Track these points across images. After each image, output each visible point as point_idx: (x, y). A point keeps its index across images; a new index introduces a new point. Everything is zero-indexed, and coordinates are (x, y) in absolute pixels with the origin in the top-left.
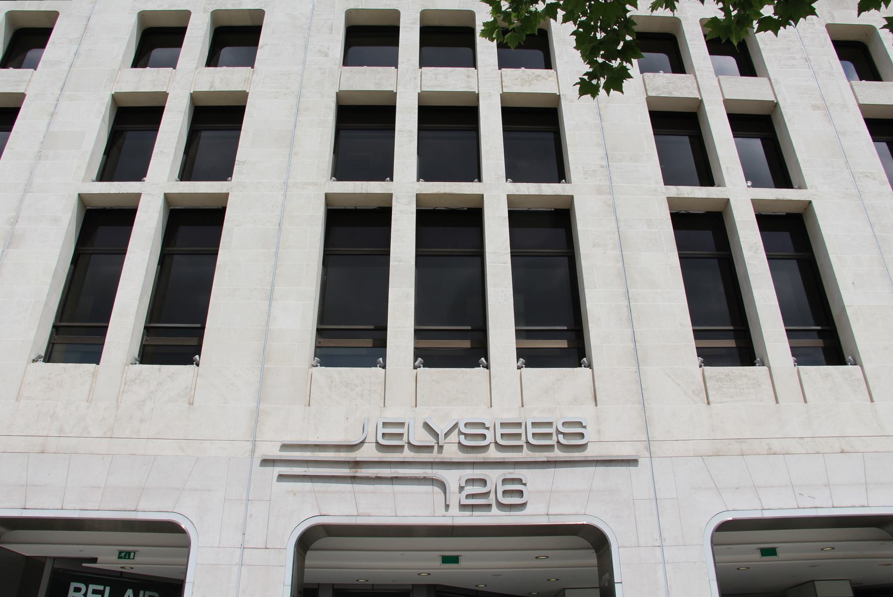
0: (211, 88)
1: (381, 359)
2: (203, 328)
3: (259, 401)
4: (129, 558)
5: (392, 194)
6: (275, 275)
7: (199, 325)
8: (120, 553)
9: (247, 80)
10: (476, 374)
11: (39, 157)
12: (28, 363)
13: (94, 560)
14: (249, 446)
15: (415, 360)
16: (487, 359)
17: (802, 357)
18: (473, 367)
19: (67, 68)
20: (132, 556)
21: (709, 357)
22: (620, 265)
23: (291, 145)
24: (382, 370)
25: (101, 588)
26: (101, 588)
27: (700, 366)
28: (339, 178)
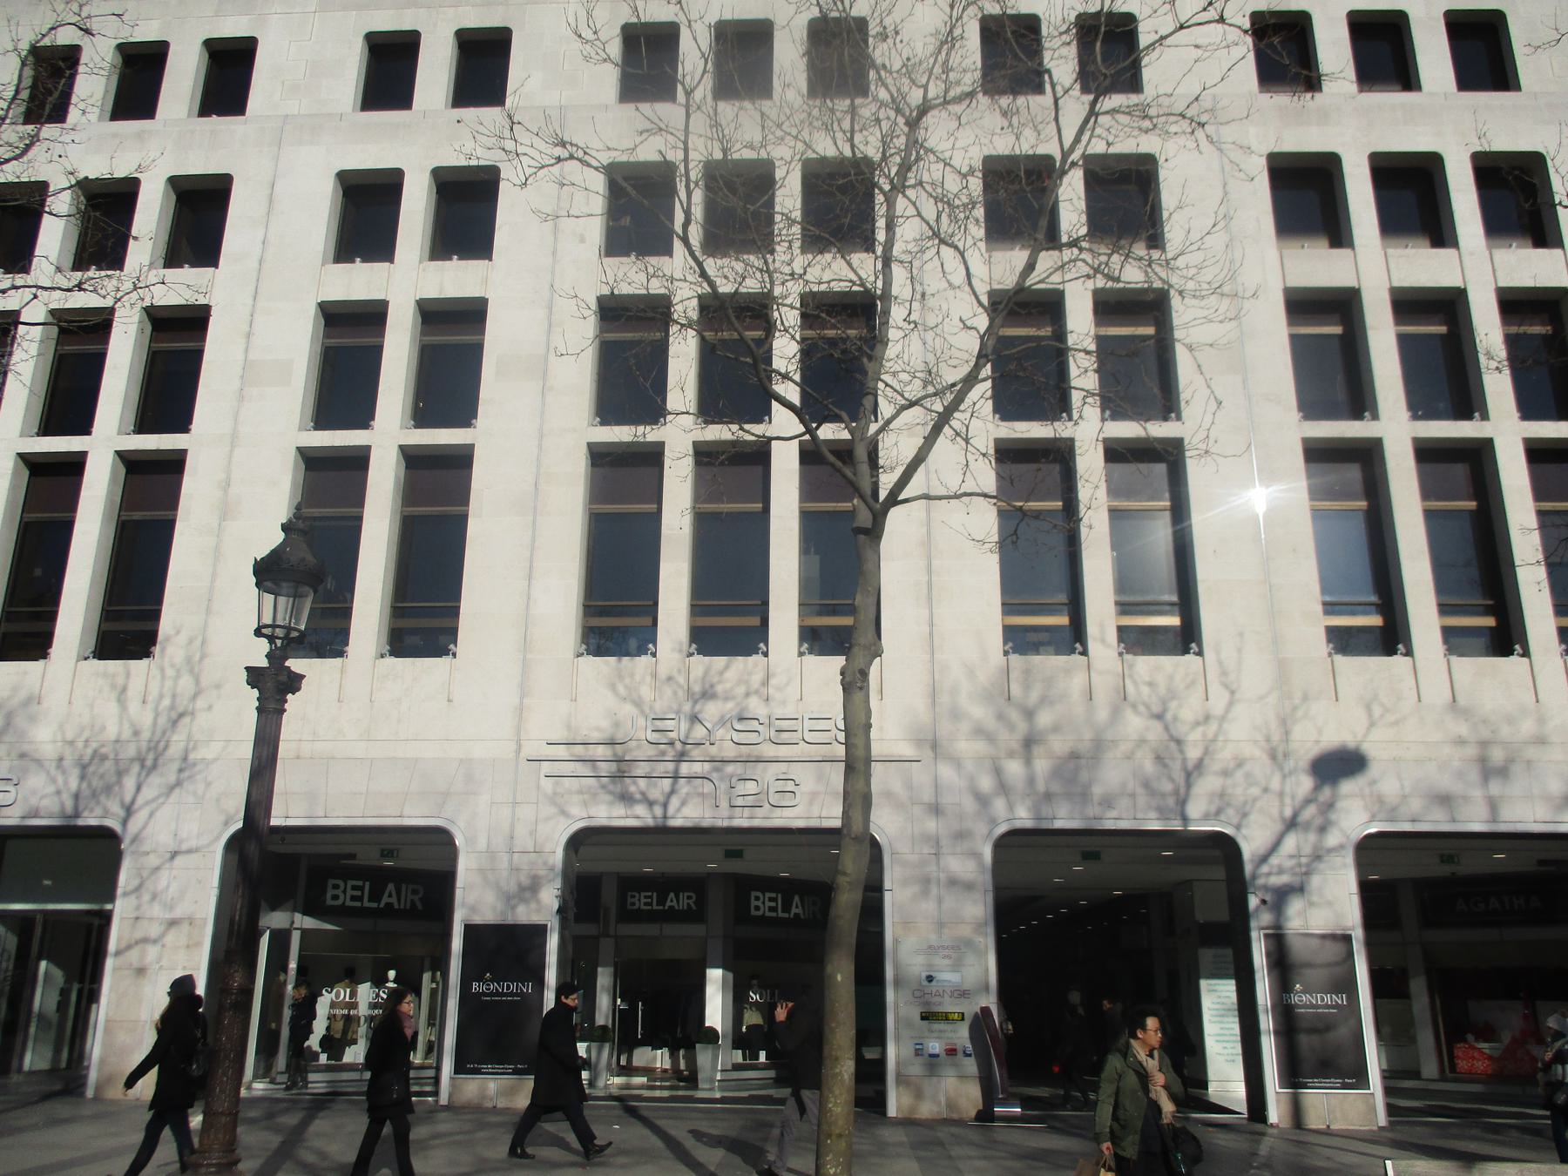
0: (441, 293)
1: (651, 646)
2: (656, 604)
3: (522, 698)
4: (392, 856)
5: (664, 443)
6: (533, 549)
7: (651, 603)
8: (383, 851)
9: (485, 281)
10: (1398, 662)
11: (241, 397)
12: (78, 661)
13: (352, 856)
14: (513, 746)
15: (800, 645)
16: (767, 646)
17: (1454, 640)
18: (750, 655)
19: (256, 265)
20: (395, 854)
21: (1344, 641)
22: (924, 530)
23: (545, 375)
24: (1198, 658)
25: (360, 883)
26: (360, 883)
27: (1445, 655)
28: (605, 422)
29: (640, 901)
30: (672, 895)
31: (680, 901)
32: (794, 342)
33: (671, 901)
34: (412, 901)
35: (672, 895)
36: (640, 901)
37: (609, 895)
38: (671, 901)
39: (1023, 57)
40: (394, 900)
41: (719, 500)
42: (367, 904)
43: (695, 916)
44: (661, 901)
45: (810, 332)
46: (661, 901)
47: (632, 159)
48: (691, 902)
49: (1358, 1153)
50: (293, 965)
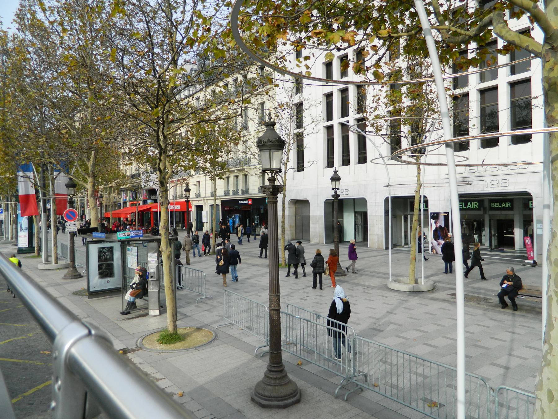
29: (495, 205)
30: (504, 203)
31: (507, 205)
32: (239, 274)
33: (503, 205)
34: (475, 206)
35: (504, 203)
36: (495, 205)
37: (486, 204)
38: (503, 205)
39: (368, 340)
40: (470, 206)
41: (45, 387)
42: (464, 208)
43: (511, 208)
44: (501, 205)
45: (263, 195)
46: (501, 205)
47: (350, 105)
48: (476, 205)
49: (492, 165)
50: (71, 215)
